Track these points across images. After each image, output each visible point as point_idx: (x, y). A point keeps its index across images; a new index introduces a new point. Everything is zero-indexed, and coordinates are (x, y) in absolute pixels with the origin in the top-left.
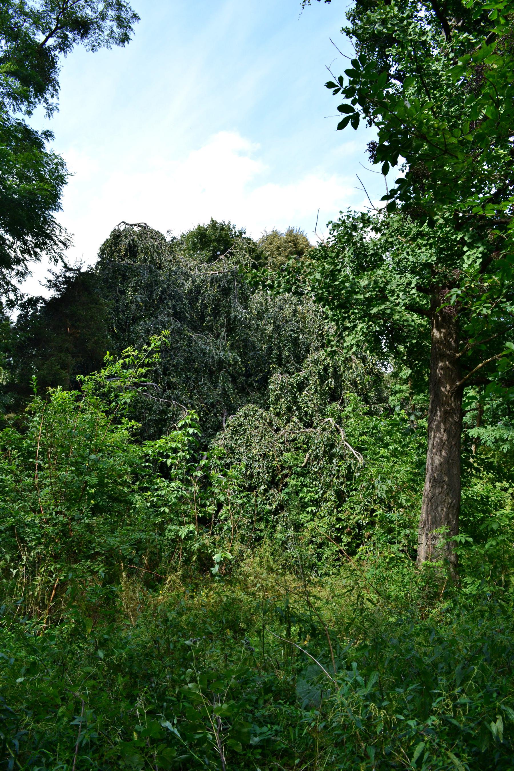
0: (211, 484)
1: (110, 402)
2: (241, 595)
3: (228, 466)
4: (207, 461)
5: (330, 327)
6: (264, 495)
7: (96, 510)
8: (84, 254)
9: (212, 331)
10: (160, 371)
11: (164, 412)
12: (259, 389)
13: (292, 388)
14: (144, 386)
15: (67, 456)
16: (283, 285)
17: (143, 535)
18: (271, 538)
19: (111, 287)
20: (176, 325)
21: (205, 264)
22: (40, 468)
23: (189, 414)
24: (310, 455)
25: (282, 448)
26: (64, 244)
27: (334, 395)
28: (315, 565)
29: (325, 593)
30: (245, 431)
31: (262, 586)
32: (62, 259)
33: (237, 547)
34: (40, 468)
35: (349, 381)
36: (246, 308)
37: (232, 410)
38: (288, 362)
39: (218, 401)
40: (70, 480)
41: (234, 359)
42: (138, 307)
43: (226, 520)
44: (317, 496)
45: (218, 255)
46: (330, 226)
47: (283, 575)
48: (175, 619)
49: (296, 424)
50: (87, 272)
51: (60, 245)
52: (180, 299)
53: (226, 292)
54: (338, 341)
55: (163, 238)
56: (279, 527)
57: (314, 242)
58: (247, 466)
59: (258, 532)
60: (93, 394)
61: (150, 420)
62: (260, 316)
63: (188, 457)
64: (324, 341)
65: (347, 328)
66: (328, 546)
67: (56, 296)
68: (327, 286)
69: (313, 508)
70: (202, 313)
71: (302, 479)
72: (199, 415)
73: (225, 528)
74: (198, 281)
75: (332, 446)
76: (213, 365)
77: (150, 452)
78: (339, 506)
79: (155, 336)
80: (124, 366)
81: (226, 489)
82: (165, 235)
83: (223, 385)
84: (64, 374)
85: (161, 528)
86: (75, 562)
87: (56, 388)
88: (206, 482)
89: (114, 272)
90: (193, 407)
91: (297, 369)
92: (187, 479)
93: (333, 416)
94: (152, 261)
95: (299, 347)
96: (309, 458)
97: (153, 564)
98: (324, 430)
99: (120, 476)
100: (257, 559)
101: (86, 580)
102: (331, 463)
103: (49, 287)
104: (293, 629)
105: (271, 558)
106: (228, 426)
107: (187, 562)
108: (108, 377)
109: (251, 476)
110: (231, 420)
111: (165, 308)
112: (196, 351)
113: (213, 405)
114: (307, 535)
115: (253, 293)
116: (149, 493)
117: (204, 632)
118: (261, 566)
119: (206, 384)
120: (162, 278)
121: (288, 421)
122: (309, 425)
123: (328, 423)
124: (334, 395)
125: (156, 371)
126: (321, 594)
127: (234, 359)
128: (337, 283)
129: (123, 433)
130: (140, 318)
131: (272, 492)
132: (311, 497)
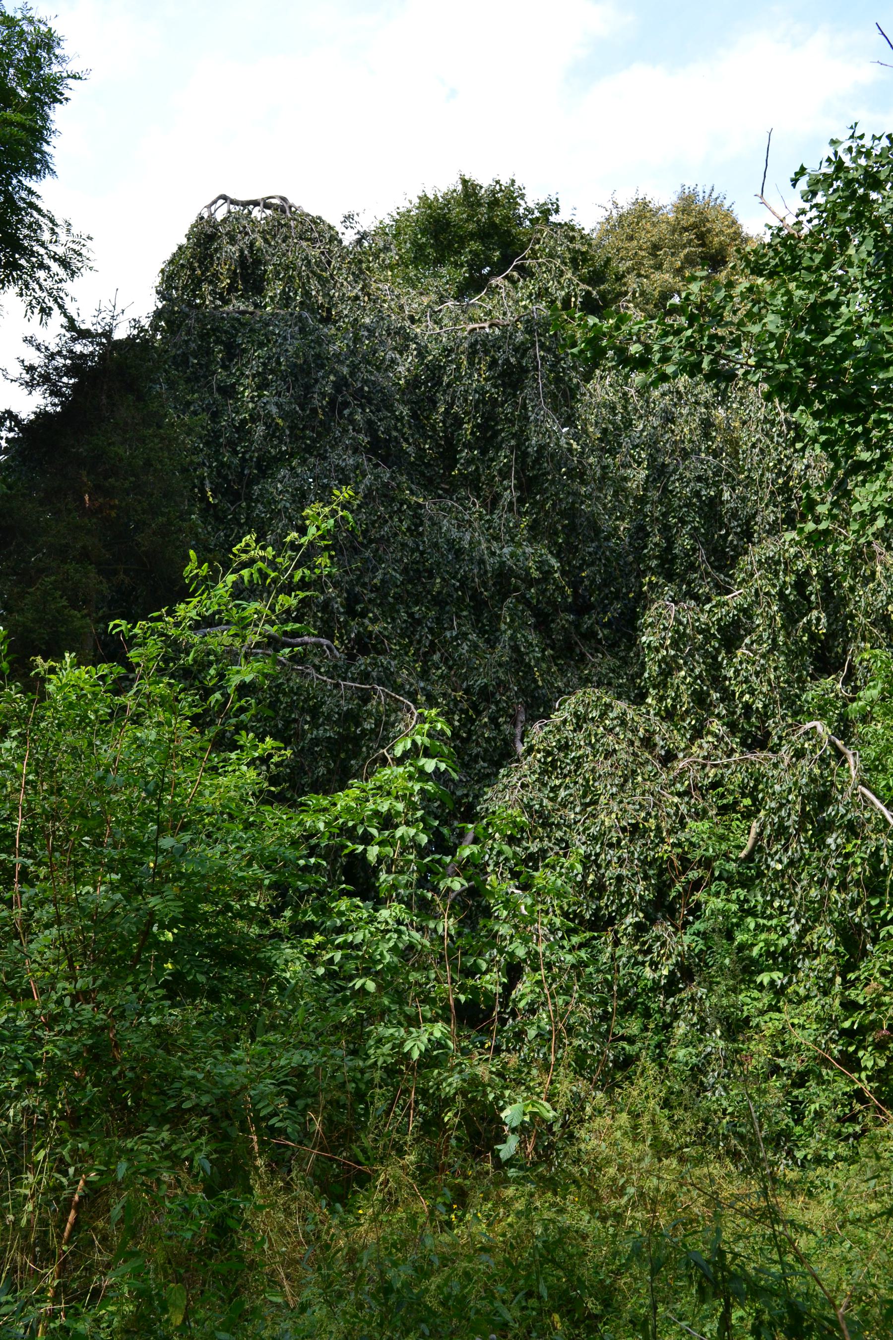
0: (487, 912)
1: (207, 693)
2: (585, 1221)
3: (534, 860)
4: (475, 848)
5: (812, 464)
6: (636, 939)
7: (177, 989)
8: (120, 288)
9: (477, 490)
10: (337, 605)
11: (353, 717)
12: (613, 646)
13: (707, 640)
14: (292, 646)
15: (97, 842)
16: (676, 356)
17: (310, 1057)
18: (660, 1058)
19: (198, 378)
20: (377, 477)
21: (450, 303)
22: (26, 877)
23: (422, 719)
24: (763, 827)
25: (683, 809)
26: (64, 263)
27: (826, 657)
28: (786, 1134)
29: (817, 1214)
30: (578, 763)
31: (642, 1195)
32: (61, 307)
33: (567, 1086)
34: (26, 877)
35: (867, 615)
36: (569, 421)
37: (539, 707)
38: (692, 567)
39: (500, 683)
40: (107, 909)
41: (542, 564)
42: (273, 431)
43: (533, 1011)
44: (784, 942)
45: (486, 278)
46: (803, 184)
47: (700, 1161)
48: (407, 1285)
49: (720, 739)
50: (130, 340)
51: (55, 267)
52: (387, 404)
53: (512, 378)
54: (835, 504)
55: (335, 238)
56: (681, 1029)
57: (756, 225)
58: (588, 861)
59: (625, 1044)
60: (161, 671)
61: (316, 741)
62: (609, 443)
63: (424, 839)
64: (794, 505)
65: (859, 466)
66: (821, 1081)
67: (49, 409)
68: (803, 350)
69: (776, 975)
70: (449, 440)
71: (742, 893)
72: (449, 722)
73: (532, 1033)
74: (435, 350)
75: (824, 799)
76: (484, 584)
77: (321, 826)
78: (850, 966)
79: (317, 506)
80: (240, 592)
81: (530, 924)
82: (339, 228)
83: (513, 638)
84: (79, 619)
85: (356, 1036)
86: (127, 1134)
87: (60, 658)
88: (473, 907)
89: (203, 337)
90: (431, 702)
91: (717, 586)
92: (423, 899)
93: (823, 716)
94: (307, 304)
95: (722, 526)
96: (760, 834)
97: (340, 1135)
98: (799, 754)
99: (241, 896)
100: (624, 1118)
101: (159, 1181)
102: (822, 844)
103: (30, 385)
104: (737, 1313)
105: (662, 1115)
106: (530, 750)
107: (432, 1126)
108: (196, 626)
109: (599, 888)
110: (537, 733)
111: (345, 431)
112: (436, 545)
113: (486, 694)
114: (759, 1051)
115: (587, 377)
116: (318, 938)
117: (491, 1322)
118: (635, 1137)
119: (464, 636)
120: (333, 348)
121: (698, 732)
122: (758, 741)
123: (810, 734)
124: (826, 657)
125: (326, 606)
126: (808, 1216)
127: (542, 564)
128: (829, 340)
129: (242, 776)
130: (280, 460)
131: (657, 930)
132: (767, 943)
